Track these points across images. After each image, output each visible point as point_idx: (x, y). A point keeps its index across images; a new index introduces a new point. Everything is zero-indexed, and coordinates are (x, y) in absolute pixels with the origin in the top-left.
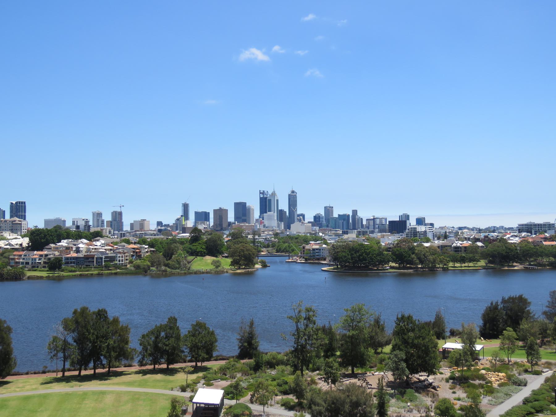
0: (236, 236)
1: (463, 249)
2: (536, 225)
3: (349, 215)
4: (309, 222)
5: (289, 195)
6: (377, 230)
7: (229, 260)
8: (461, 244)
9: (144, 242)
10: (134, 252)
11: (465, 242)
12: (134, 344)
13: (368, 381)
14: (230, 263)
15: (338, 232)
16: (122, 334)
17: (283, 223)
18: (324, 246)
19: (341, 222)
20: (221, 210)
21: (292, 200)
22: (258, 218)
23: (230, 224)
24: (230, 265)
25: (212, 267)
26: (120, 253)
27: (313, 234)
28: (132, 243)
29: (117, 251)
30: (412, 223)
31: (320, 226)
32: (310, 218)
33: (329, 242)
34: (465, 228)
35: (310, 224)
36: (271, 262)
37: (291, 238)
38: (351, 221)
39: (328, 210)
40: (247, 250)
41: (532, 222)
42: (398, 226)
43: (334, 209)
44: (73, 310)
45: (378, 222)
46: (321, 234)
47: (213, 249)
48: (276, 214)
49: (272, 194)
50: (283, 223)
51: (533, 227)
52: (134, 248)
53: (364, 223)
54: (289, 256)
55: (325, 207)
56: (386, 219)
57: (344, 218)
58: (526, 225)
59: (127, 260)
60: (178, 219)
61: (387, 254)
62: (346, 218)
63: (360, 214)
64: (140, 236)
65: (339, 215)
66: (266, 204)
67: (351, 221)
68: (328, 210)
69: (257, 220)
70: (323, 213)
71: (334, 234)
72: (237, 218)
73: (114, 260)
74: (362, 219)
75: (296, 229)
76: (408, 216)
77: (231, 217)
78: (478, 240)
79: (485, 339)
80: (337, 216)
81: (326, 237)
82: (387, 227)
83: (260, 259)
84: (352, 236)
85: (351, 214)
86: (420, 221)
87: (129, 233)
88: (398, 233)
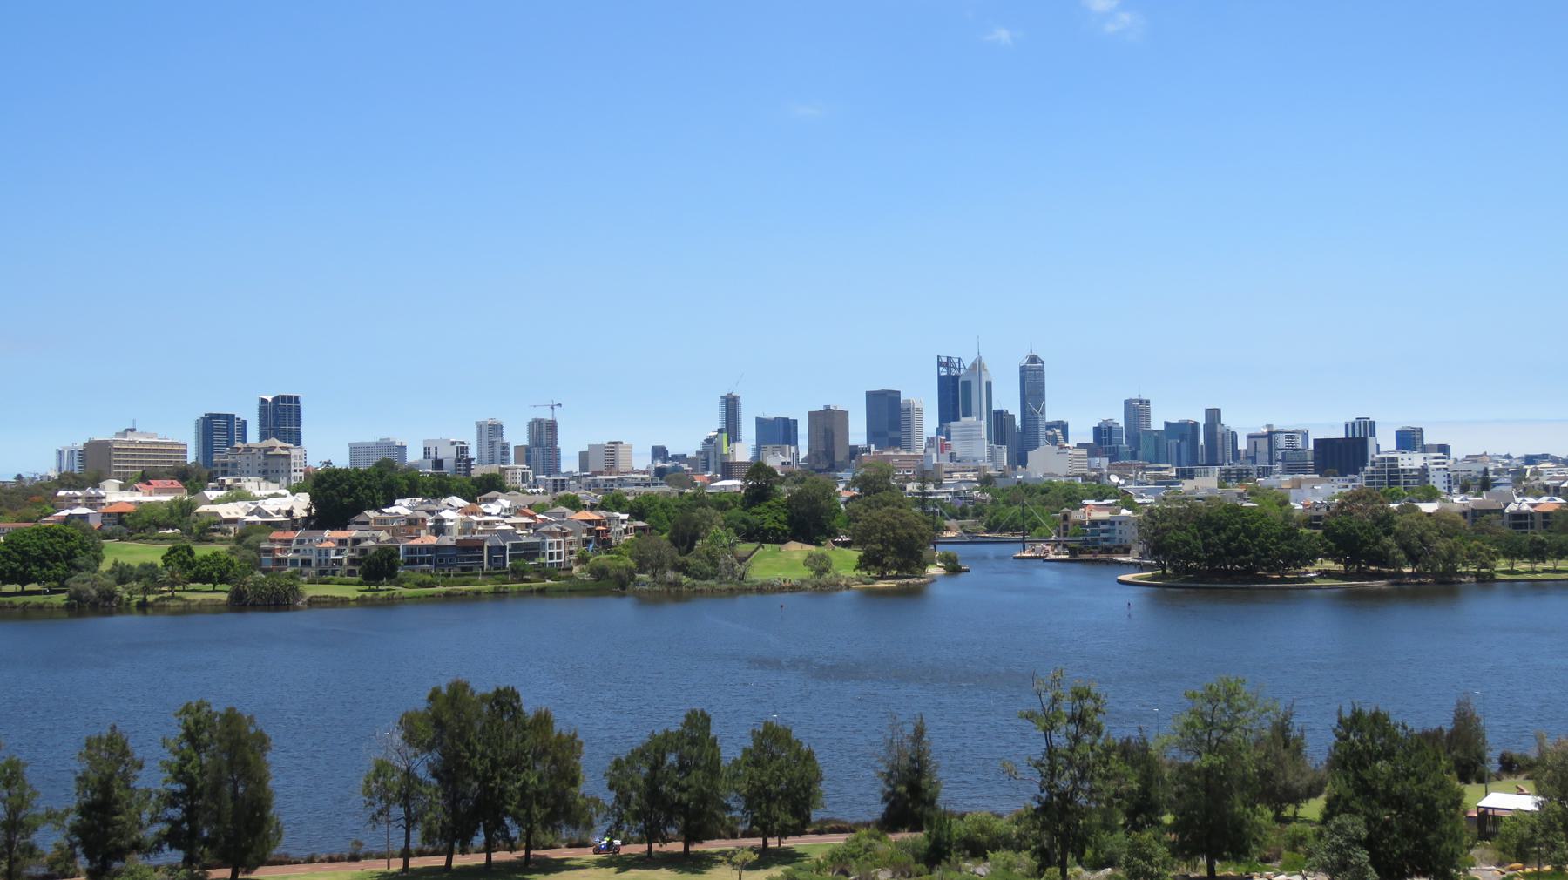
0: (873, 486)
1: (1539, 521)
3: (1196, 424)
4: (1080, 446)
5: (1023, 369)
7: (854, 554)
9: (617, 503)
10: (589, 531)
11: (1544, 499)
12: (593, 785)
15: (1164, 473)
16: (562, 757)
17: (1004, 448)
18: (1124, 512)
19: (1173, 442)
20: (828, 412)
21: (1032, 381)
22: (933, 433)
24: (857, 568)
26: (552, 534)
27: (1094, 478)
29: (546, 528)
30: (1384, 443)
31: (1114, 455)
32: (1082, 432)
33: (1139, 501)
34: (1545, 457)
35: (1084, 451)
36: (973, 558)
37: (1028, 489)
38: (1202, 440)
39: (1137, 410)
42: (1342, 454)
45: (1282, 442)
46: (1114, 479)
47: (808, 522)
48: (984, 423)
49: (974, 365)
50: (1004, 448)
53: (1242, 445)
54: (1023, 542)
55: (1127, 403)
56: (1306, 435)
57: (1182, 431)
59: (571, 553)
60: (710, 441)
61: (1310, 536)
62: (1189, 432)
63: (1229, 421)
64: (607, 487)
65: (1167, 424)
66: (956, 393)
67: (1202, 440)
68: (1137, 410)
69: (931, 441)
70: (1120, 420)
71: (1152, 477)
72: (874, 435)
73: (537, 555)
74: (1234, 436)
75: (1044, 464)
76: (1373, 424)
77: (858, 434)
81: (1131, 488)
82: (1310, 456)
83: (941, 550)
84: (1205, 484)
85: (1202, 421)
86: (1408, 440)
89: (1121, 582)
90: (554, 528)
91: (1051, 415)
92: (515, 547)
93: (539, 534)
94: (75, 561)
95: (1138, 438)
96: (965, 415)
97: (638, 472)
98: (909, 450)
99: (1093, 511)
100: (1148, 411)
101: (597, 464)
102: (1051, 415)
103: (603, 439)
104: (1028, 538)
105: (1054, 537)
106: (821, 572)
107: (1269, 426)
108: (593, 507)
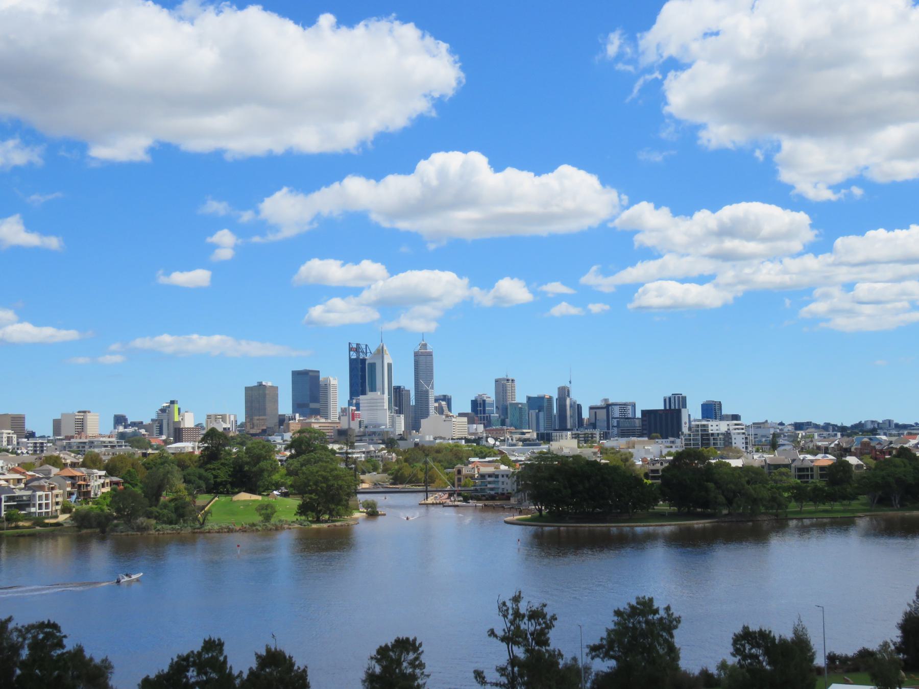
0: (303, 445)
1: (816, 473)
3: (550, 399)
4: (461, 415)
5: (416, 355)
6: (615, 430)
7: (294, 502)
8: (812, 461)
9: (92, 462)
10: (73, 485)
11: (820, 456)
14: (295, 508)
15: (527, 436)
17: (402, 416)
19: (533, 413)
21: (423, 364)
23: (282, 420)
25: (257, 519)
26: (41, 488)
28: (65, 465)
29: (36, 483)
30: (692, 413)
31: (487, 422)
33: (513, 458)
34: (809, 424)
35: (465, 419)
39: (503, 386)
40: (337, 477)
42: (663, 422)
43: (516, 383)
44: (473, 675)
45: (616, 412)
46: (491, 441)
47: (246, 476)
48: (386, 396)
49: (378, 350)
50: (402, 416)
53: (586, 415)
54: (426, 491)
55: (497, 381)
59: (57, 503)
60: (163, 410)
61: (652, 484)
64: (79, 449)
65: (529, 398)
66: (362, 375)
68: (503, 386)
71: (520, 440)
72: (298, 406)
73: (28, 505)
74: (579, 407)
75: (431, 431)
76: (684, 399)
77: (285, 406)
78: (848, 451)
79: (407, 639)
81: (504, 448)
83: (361, 498)
85: (555, 396)
86: (711, 410)
87: (54, 442)
88: (665, 436)
89: (506, 522)
90: (42, 482)
92: (10, 499)
93: (30, 489)
95: (507, 409)
99: (479, 466)
100: (513, 387)
102: (437, 390)
103: (73, 408)
104: (429, 488)
106: (267, 518)
107: (606, 400)
108: (73, 465)
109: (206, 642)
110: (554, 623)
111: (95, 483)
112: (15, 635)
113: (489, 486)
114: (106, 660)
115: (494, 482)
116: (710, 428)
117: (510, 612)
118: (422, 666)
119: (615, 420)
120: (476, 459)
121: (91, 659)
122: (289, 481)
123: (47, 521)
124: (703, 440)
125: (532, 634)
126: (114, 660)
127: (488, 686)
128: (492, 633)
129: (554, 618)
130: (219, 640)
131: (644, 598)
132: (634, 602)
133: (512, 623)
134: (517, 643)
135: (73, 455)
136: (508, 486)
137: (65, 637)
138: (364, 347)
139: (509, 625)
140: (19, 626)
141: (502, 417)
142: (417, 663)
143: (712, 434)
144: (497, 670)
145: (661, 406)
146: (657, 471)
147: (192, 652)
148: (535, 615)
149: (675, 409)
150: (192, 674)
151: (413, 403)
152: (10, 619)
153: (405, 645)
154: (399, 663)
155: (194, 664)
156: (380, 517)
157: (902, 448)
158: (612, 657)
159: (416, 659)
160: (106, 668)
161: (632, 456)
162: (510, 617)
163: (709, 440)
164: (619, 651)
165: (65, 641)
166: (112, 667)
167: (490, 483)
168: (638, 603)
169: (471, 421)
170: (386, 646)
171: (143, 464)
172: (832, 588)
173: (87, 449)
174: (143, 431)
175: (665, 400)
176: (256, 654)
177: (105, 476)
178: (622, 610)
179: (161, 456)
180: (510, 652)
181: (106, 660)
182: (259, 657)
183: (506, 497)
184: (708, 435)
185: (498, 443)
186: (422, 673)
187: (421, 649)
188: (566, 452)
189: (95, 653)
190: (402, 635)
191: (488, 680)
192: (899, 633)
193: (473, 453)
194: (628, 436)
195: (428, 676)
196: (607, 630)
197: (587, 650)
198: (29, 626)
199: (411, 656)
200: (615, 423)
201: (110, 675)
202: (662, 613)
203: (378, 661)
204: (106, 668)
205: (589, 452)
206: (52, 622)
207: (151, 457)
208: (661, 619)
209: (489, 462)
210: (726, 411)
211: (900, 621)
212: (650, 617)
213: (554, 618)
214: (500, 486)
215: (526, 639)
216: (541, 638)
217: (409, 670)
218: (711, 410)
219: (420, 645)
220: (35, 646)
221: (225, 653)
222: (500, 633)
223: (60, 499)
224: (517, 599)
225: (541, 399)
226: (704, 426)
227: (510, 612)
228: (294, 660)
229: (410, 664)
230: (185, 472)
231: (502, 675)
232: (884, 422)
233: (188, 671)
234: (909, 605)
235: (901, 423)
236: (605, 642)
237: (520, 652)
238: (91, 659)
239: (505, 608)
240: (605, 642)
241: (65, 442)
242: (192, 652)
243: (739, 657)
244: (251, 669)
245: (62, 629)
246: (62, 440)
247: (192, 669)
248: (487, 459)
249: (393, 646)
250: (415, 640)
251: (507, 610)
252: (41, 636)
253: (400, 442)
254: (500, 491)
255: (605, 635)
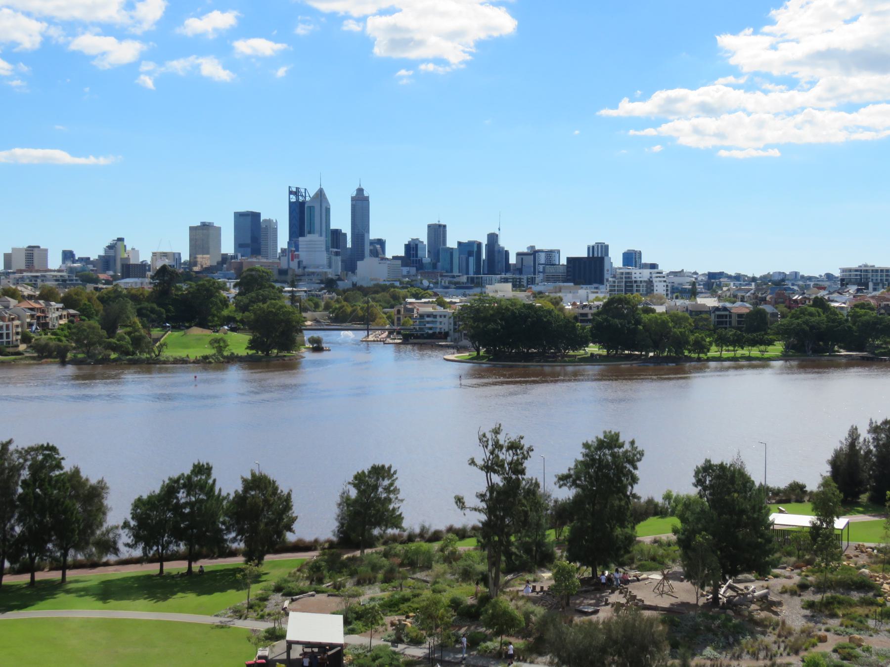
2: (877, 271)
4: (395, 258)
5: (353, 199)
9: (47, 296)
10: (32, 316)
12: (118, 512)
13: (634, 593)
16: (92, 497)
20: (205, 226)
21: (360, 205)
22: (286, 246)
24: (248, 348)
28: (23, 297)
30: (616, 260)
32: (395, 249)
33: (448, 300)
35: (399, 262)
38: (484, 256)
39: (437, 232)
41: (870, 263)
42: (588, 268)
44: (454, 500)
45: (542, 258)
48: (323, 238)
49: (316, 194)
51: (870, 275)
52: (32, 309)
53: (513, 260)
54: (368, 330)
57: (469, 249)
58: (856, 271)
59: (17, 333)
62: (475, 249)
63: (503, 242)
65: (460, 244)
68: (437, 232)
69: (283, 251)
70: (424, 238)
74: (507, 253)
75: (368, 271)
77: (228, 246)
80: (455, 246)
85: (484, 242)
91: (373, 235)
94: (805, 635)
96: (310, 233)
97: (54, 271)
98: (267, 257)
101: (20, 263)
102: (373, 235)
105: (388, 327)
106: (220, 350)
107: (532, 247)
109: (195, 466)
110: (530, 453)
111: (53, 315)
112: (15, 456)
113: (428, 325)
114: (102, 481)
115: (432, 322)
116: (633, 276)
117: (490, 443)
118: (396, 491)
119: (541, 267)
120: (413, 300)
121: (87, 480)
122: (239, 316)
123: (8, 350)
124: (626, 286)
125: (510, 464)
126: (109, 482)
127: (467, 511)
128: (472, 462)
129: (531, 449)
130: (207, 464)
131: (610, 432)
132: (601, 437)
133: (492, 453)
134: (495, 472)
135: (29, 288)
136: (444, 325)
137: (63, 459)
138: (303, 191)
139: (488, 454)
140: (19, 449)
141: (434, 261)
142: (392, 488)
143: (636, 282)
144: (477, 496)
145: (584, 254)
146: (586, 315)
147: (183, 474)
148: (514, 446)
149: (598, 257)
150: (182, 495)
151: (349, 245)
152: (10, 442)
153: (380, 471)
154: (376, 487)
155: (184, 486)
156: (325, 353)
157: (816, 298)
158: (577, 486)
159: (391, 484)
160: (103, 488)
161: (561, 300)
162: (490, 447)
163: (632, 286)
164: (585, 480)
165: (63, 463)
166: (108, 488)
167: (428, 322)
168: (605, 437)
169: (404, 265)
170: (363, 472)
171: (98, 298)
172: (778, 425)
173: (39, 282)
174: (91, 267)
175: (589, 248)
176: (242, 478)
177: (63, 309)
178: (590, 442)
179: (115, 291)
180: (489, 479)
181: (102, 481)
182: (245, 481)
183: (445, 336)
184: (631, 282)
185: (432, 285)
186: (397, 498)
187: (395, 476)
188: (499, 295)
189: (91, 475)
190: (379, 463)
191: (467, 504)
192: (829, 468)
193: (409, 294)
194: (555, 281)
195: (402, 501)
196: (576, 461)
197: (556, 479)
198: (29, 448)
199: (386, 482)
200: (541, 268)
201: (105, 495)
202: (627, 447)
203: (355, 486)
204: (103, 488)
205: (523, 297)
206: (51, 445)
207: (104, 291)
208: (627, 451)
209: (425, 303)
210: (645, 260)
211: (830, 458)
212: (616, 450)
213: (531, 449)
214: (438, 325)
215: (502, 466)
216: (517, 468)
217: (384, 495)
218: (631, 258)
219: (395, 472)
220: (36, 469)
221: (213, 476)
222: (480, 462)
223: (19, 330)
224: (497, 431)
225: (471, 244)
226: (628, 273)
227: (490, 443)
228: (277, 484)
229: (385, 489)
230: (138, 306)
231: (482, 501)
232: (791, 273)
233: (179, 492)
234: (841, 442)
235: (806, 275)
236: (572, 472)
237: (497, 479)
238: (87, 480)
239: (485, 439)
240: (572, 472)
241: (18, 275)
242: (183, 474)
243: (700, 488)
244: (236, 492)
245: (60, 452)
246: (14, 273)
247: (182, 491)
248: (423, 300)
249: (370, 472)
250: (390, 468)
251: (487, 441)
252: (40, 457)
253: (339, 282)
254: (438, 331)
255: (572, 466)
